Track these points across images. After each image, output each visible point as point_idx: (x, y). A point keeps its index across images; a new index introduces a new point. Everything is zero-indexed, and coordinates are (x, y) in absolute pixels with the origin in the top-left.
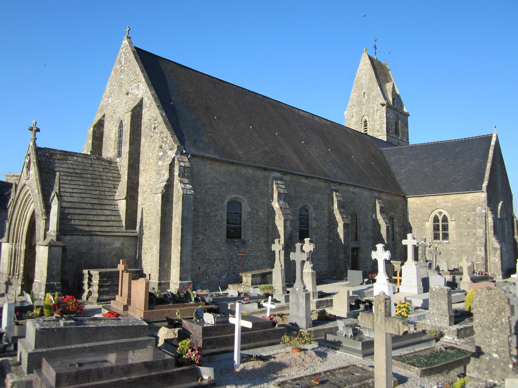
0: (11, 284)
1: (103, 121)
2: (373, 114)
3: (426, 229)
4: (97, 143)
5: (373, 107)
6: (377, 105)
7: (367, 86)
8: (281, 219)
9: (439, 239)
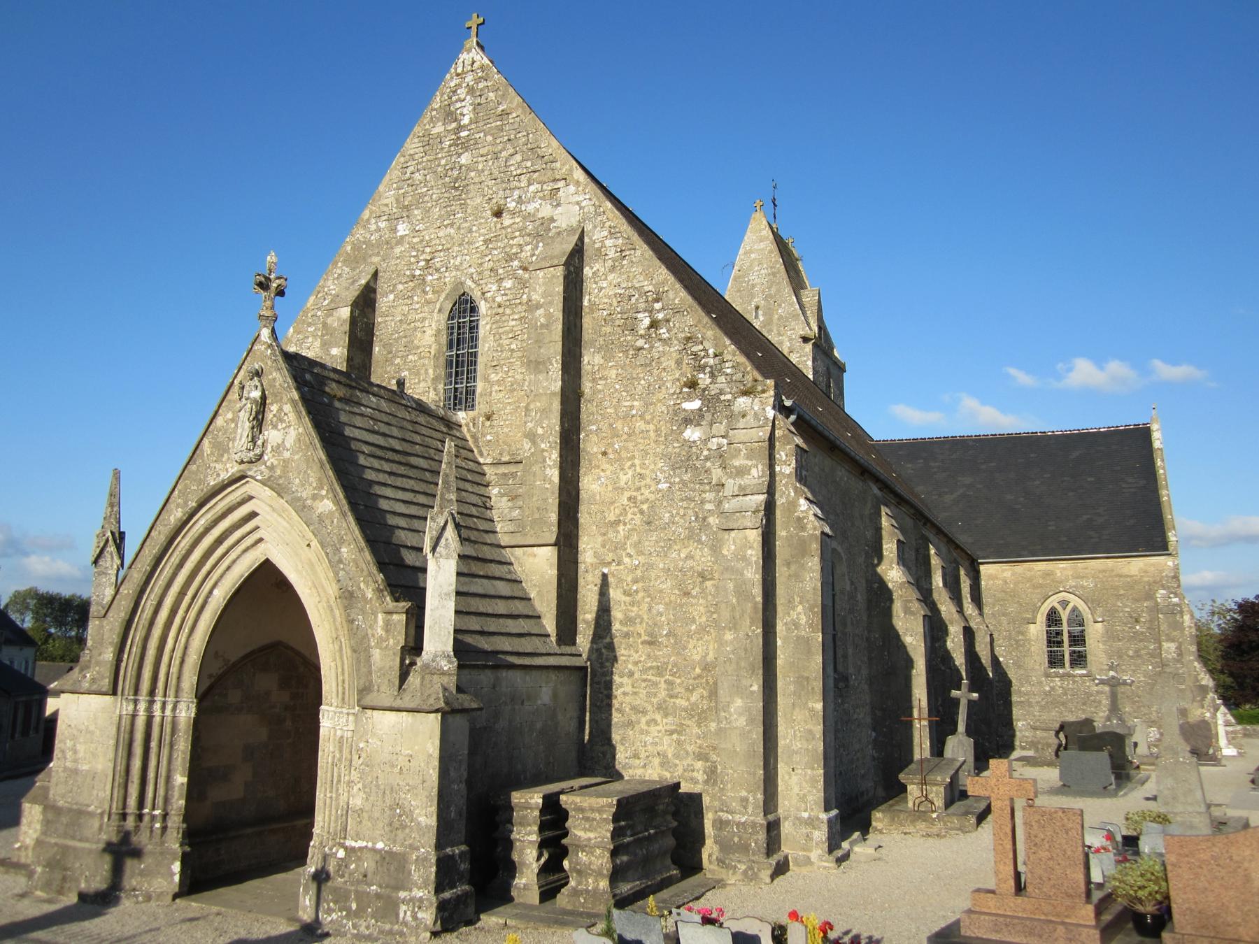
0: (137, 853)
1: (374, 291)
3: (1029, 640)
4: (357, 361)
6: (791, 339)
7: (763, 292)
8: (912, 613)
9: (1063, 666)
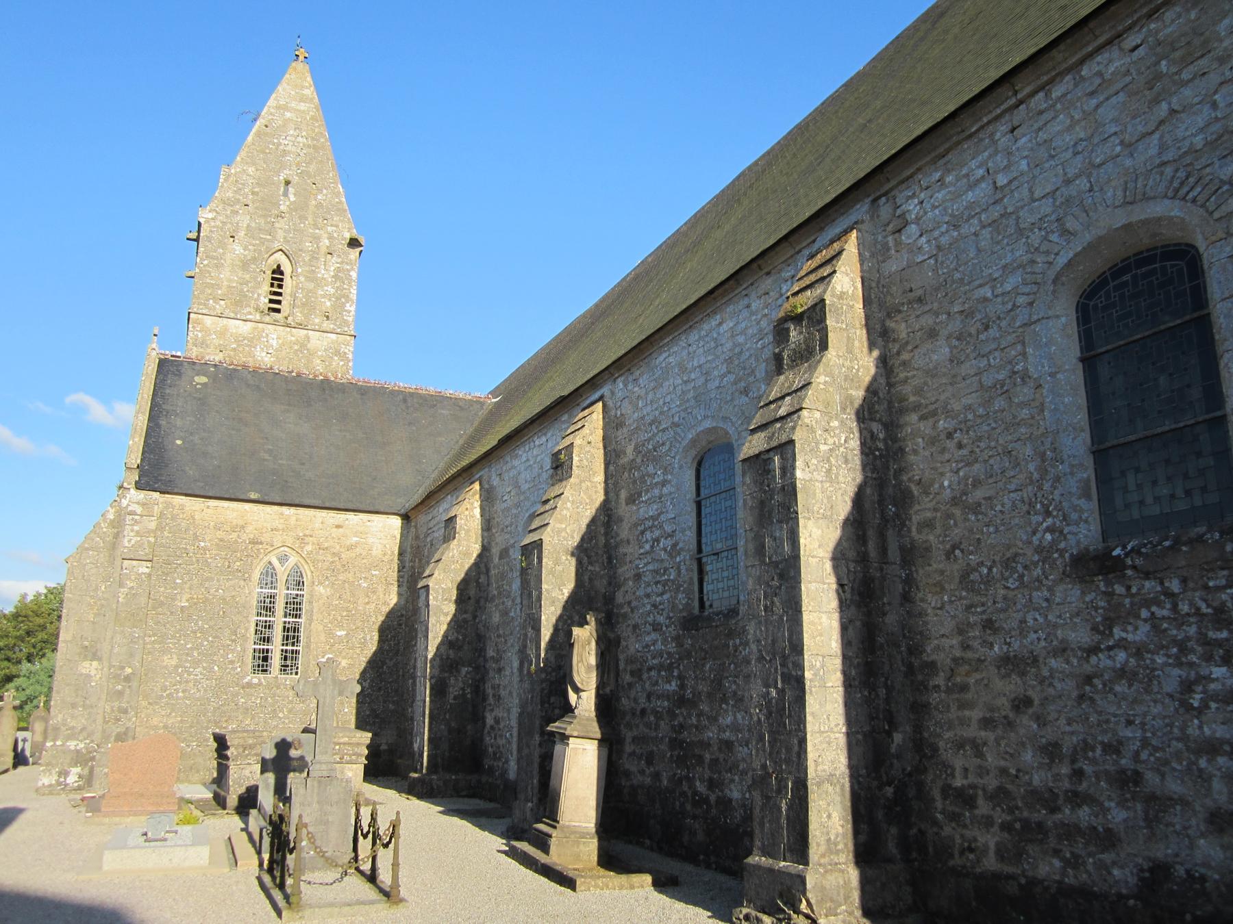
2: (314, 258)
5: (317, 239)
7: (298, 165)
